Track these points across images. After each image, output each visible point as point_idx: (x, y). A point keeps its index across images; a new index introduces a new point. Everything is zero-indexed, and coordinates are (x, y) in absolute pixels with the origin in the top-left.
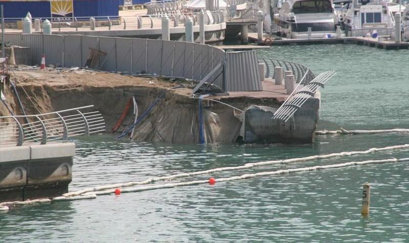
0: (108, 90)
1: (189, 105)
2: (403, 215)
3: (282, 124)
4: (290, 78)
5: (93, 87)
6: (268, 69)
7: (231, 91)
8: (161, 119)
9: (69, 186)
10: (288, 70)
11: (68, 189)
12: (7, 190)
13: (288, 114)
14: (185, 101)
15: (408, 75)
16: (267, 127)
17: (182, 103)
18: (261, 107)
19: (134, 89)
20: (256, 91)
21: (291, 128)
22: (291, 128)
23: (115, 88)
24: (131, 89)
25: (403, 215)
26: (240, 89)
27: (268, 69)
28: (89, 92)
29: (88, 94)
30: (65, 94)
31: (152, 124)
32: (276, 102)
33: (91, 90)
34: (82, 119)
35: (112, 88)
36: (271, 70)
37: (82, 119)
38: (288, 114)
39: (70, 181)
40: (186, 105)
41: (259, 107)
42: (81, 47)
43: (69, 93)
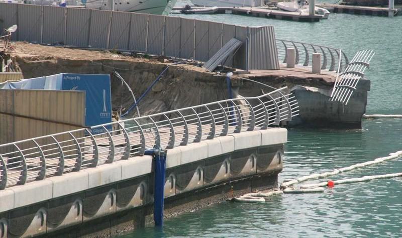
0: (86, 64)
1: (214, 83)
2: (398, 227)
3: (328, 107)
4: (317, 57)
5: (68, 60)
6: (325, 57)
7: (251, 69)
8: (176, 98)
9: (279, 178)
10: (316, 52)
11: (277, 181)
12: (243, 179)
13: (336, 95)
14: (208, 78)
15: (401, 34)
16: (313, 110)
17: (202, 80)
18: (308, 88)
19: (114, 63)
20: (274, 69)
21: (339, 111)
22: (339, 111)
23: (94, 61)
24: (110, 63)
25: (398, 227)
26: (262, 68)
27: (325, 57)
28: (64, 66)
29: (63, 67)
30: (37, 67)
31: (165, 102)
32: (323, 82)
33: (66, 63)
34: (222, 115)
35: (91, 62)
36: (328, 61)
37: (222, 115)
38: (336, 95)
39: (280, 171)
40: (210, 84)
41: (306, 87)
42: (17, 16)
43: (40, 65)
